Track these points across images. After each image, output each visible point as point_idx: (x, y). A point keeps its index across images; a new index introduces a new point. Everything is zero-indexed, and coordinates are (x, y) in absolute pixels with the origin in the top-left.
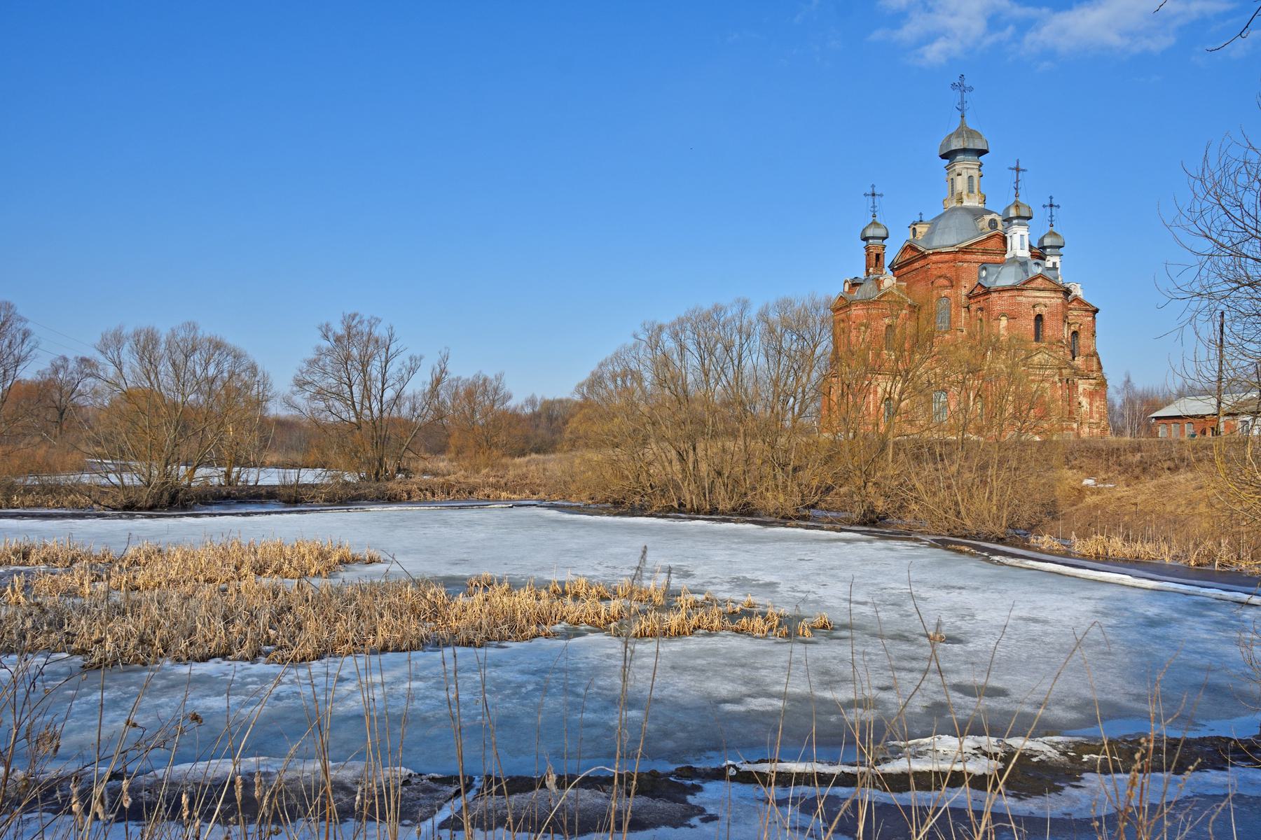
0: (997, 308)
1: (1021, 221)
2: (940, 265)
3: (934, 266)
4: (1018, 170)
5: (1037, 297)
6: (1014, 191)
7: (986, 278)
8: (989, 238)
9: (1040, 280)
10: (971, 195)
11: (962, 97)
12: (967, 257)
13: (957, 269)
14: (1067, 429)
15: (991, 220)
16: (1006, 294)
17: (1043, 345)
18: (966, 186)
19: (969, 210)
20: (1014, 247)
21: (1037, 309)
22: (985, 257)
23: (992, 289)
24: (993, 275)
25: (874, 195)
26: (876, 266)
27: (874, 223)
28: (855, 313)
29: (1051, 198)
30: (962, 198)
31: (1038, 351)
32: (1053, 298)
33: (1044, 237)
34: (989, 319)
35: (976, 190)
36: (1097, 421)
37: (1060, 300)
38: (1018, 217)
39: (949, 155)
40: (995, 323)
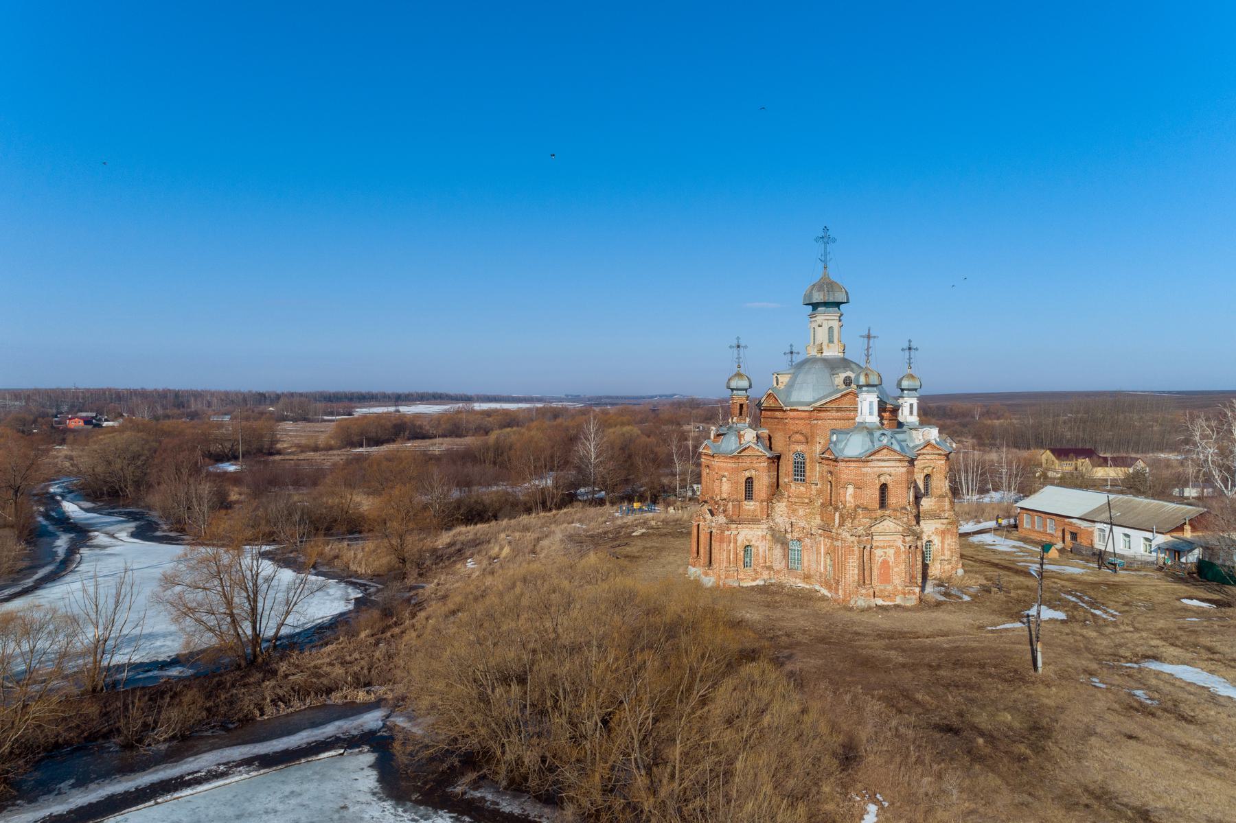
1: (870, 389)
2: (797, 422)
3: (791, 421)
4: (869, 337)
5: (883, 467)
7: (835, 444)
9: (885, 450)
10: (831, 345)
11: (825, 248)
12: (822, 414)
14: (909, 593)
15: (846, 377)
16: (853, 465)
17: (887, 512)
18: (827, 336)
19: (826, 361)
20: (864, 411)
22: (839, 414)
23: (839, 459)
26: (741, 414)
27: (739, 375)
28: (718, 464)
30: (822, 349)
31: (883, 518)
33: (902, 379)
35: (836, 340)
36: (949, 557)
37: (904, 470)
38: (868, 385)
39: (815, 306)
40: (841, 491)
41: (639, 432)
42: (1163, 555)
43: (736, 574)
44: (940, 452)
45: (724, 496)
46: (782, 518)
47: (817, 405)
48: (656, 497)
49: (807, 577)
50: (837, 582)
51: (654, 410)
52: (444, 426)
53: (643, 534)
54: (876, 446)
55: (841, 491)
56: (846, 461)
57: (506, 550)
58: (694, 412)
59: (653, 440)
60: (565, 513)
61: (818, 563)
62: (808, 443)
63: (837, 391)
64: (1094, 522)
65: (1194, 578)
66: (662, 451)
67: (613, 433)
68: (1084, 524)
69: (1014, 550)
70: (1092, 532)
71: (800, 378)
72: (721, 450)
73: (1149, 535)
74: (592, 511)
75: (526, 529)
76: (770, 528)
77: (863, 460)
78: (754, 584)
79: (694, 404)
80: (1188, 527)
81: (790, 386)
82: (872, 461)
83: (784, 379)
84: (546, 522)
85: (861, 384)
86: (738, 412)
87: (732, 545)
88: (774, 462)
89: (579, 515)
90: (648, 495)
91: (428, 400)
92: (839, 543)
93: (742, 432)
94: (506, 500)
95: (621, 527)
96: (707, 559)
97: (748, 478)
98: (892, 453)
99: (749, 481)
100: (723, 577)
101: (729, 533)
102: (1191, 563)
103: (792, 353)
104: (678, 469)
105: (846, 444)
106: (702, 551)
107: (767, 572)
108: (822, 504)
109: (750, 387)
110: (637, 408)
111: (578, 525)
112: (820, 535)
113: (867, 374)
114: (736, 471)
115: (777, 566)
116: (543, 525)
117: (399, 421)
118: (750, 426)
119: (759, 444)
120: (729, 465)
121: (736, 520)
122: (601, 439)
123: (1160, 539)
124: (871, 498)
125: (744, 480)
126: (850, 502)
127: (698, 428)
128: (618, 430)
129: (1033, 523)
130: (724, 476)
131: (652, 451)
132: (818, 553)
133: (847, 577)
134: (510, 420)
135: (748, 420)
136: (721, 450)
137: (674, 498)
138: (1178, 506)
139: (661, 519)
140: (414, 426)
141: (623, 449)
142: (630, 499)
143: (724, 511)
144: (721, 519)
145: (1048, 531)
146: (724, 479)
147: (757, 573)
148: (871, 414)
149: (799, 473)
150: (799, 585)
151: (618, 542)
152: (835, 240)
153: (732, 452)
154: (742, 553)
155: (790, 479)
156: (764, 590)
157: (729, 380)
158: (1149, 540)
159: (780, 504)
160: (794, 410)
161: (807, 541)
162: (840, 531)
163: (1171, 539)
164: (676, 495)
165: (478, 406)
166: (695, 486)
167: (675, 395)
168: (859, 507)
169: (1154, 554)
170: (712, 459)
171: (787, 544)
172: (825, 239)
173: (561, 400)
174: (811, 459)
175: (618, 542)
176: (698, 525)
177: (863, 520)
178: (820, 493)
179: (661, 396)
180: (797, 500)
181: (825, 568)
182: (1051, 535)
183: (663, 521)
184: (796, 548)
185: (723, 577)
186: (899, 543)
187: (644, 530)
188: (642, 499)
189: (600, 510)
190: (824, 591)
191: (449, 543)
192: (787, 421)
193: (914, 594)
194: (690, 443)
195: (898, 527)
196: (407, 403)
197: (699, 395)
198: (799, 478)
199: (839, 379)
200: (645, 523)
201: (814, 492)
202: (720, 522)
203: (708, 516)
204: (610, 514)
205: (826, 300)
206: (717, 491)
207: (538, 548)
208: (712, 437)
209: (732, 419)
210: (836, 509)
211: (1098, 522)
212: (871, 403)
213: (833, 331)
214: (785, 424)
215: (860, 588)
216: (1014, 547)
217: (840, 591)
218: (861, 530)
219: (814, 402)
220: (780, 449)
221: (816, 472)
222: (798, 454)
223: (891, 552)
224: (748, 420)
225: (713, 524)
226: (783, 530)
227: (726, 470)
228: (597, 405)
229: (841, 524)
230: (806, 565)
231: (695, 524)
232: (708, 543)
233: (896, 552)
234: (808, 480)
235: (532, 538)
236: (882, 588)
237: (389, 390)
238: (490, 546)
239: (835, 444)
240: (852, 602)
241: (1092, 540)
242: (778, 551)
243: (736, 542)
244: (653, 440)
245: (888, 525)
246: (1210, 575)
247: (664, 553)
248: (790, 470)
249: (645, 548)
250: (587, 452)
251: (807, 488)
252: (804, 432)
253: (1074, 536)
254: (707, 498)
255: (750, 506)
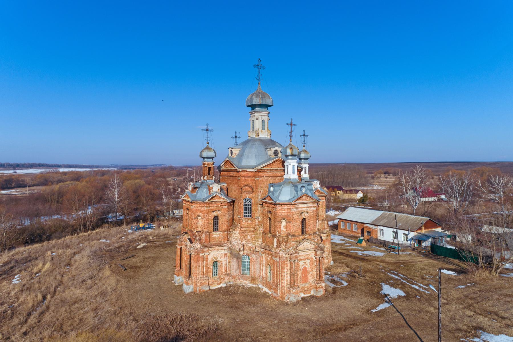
0: (280, 215)
3: (243, 178)
4: (291, 125)
6: (289, 138)
7: (273, 193)
8: (274, 162)
9: (304, 197)
10: (263, 131)
11: (259, 72)
13: (256, 181)
14: (319, 287)
15: (275, 150)
17: (306, 236)
18: (261, 126)
19: (261, 141)
21: (303, 215)
22: (271, 173)
24: (277, 191)
25: (207, 130)
26: (209, 174)
27: (208, 148)
28: (195, 208)
29: (304, 131)
30: (258, 134)
32: (311, 207)
34: (275, 221)
35: (266, 128)
36: (327, 256)
38: (292, 155)
39: (253, 107)
41: (144, 183)
42: (414, 242)
43: (207, 282)
44: (323, 195)
45: (199, 229)
46: (236, 241)
47: (259, 167)
48: (153, 217)
49: (253, 280)
50: (276, 285)
51: (153, 171)
52: (38, 180)
53: (144, 247)
54: (299, 194)
55: (278, 224)
56: (282, 205)
57: (48, 265)
58: (172, 172)
59: (151, 187)
60: (97, 233)
61: (261, 270)
62: (253, 192)
63: (270, 159)
64: (378, 226)
65: (430, 254)
66: (157, 191)
67: (128, 184)
68: (374, 227)
69: (343, 242)
70: (377, 231)
71: (247, 151)
72: (197, 198)
73: (406, 232)
74: (114, 230)
75: (68, 246)
76: (230, 249)
77: (291, 204)
78: (219, 286)
79: (171, 168)
80: (423, 228)
81: (241, 156)
82: (298, 204)
83: (236, 152)
84: (82, 240)
85: (288, 154)
86: (207, 172)
87: (205, 262)
88: (231, 205)
89: (105, 233)
90: (149, 217)
91: (35, 167)
92: (278, 259)
93: (211, 186)
94: (60, 225)
95: (131, 241)
96: (188, 274)
97: (215, 217)
98: (309, 198)
99: (216, 218)
100: (199, 285)
101: (203, 254)
102: (429, 246)
103: (236, 137)
104: (165, 201)
105: (280, 193)
106: (183, 265)
107: (228, 278)
108: (264, 232)
109: (215, 156)
110: (145, 170)
111: (104, 240)
112: (263, 252)
113: (291, 148)
114: (207, 212)
115: (234, 273)
116: (80, 243)
117: (8, 178)
118: (216, 182)
119: (222, 193)
120: (203, 208)
121: (207, 245)
122: (122, 187)
123: (412, 235)
124: (296, 228)
125: (213, 218)
126: (283, 231)
127: (174, 179)
128: (132, 182)
129: (346, 226)
130: (199, 216)
131: (151, 193)
132: (261, 263)
133: (283, 282)
134: (77, 177)
135: (214, 178)
136: (197, 198)
137: (163, 218)
138: (415, 217)
139: (156, 234)
140: (19, 180)
141: (135, 192)
142: (137, 220)
143: (200, 240)
144: (198, 245)
145: (354, 230)
146: (199, 218)
147: (221, 279)
148: (294, 173)
149: (248, 212)
150: (249, 285)
151: (127, 255)
152: (264, 68)
153: (205, 199)
154: (211, 267)
155: (242, 216)
156: (226, 291)
157: (201, 151)
158: (407, 235)
159: (235, 232)
160: (245, 171)
161: (254, 256)
162: (278, 251)
163: (417, 234)
164: (164, 216)
165: (61, 170)
166: (174, 211)
167: (163, 164)
168: (290, 235)
169: (409, 242)
170: (190, 204)
171: (240, 258)
172: (259, 66)
173: (108, 167)
174: (255, 202)
175: (127, 255)
176: (181, 248)
177: (292, 243)
178: (261, 223)
179: (156, 165)
180: (246, 229)
181: (266, 274)
182: (356, 232)
183: (156, 236)
184: (246, 261)
185: (199, 285)
186: (313, 256)
187: (145, 244)
188: (144, 220)
189: (119, 229)
190: (266, 289)
191: (7, 262)
192: (239, 178)
193: (322, 287)
194: (171, 187)
195: (312, 245)
196: (23, 168)
197: (174, 164)
198: (248, 215)
199: (271, 152)
200: (145, 238)
201: (257, 224)
202: (197, 247)
203: (189, 243)
204: (125, 231)
205: (261, 103)
206: (194, 226)
207: (73, 261)
208: (190, 189)
209: (204, 177)
210: (275, 236)
211: (380, 226)
212: (293, 166)
213: (264, 123)
214: (238, 180)
215: (292, 289)
216: (341, 240)
217: (279, 291)
218: (291, 250)
219: (257, 166)
220: (234, 196)
221: (258, 211)
222: (247, 200)
223: (308, 262)
224: (214, 178)
225: (192, 249)
226: (237, 249)
227: (201, 212)
228: (126, 169)
229: (279, 246)
230: (253, 271)
231: (179, 247)
232: (188, 262)
233: (311, 262)
234: (253, 216)
235: (70, 253)
236: (303, 286)
237: (12, 162)
238: (37, 262)
239: (273, 193)
240: (286, 298)
241: (377, 235)
242: (234, 263)
243: (207, 260)
244: (151, 187)
245: (307, 245)
246: (439, 252)
247: (158, 262)
248: (242, 210)
249: (145, 258)
250: (113, 195)
251: (252, 221)
252: (251, 185)
253: (369, 233)
254: (187, 230)
255: (216, 235)
